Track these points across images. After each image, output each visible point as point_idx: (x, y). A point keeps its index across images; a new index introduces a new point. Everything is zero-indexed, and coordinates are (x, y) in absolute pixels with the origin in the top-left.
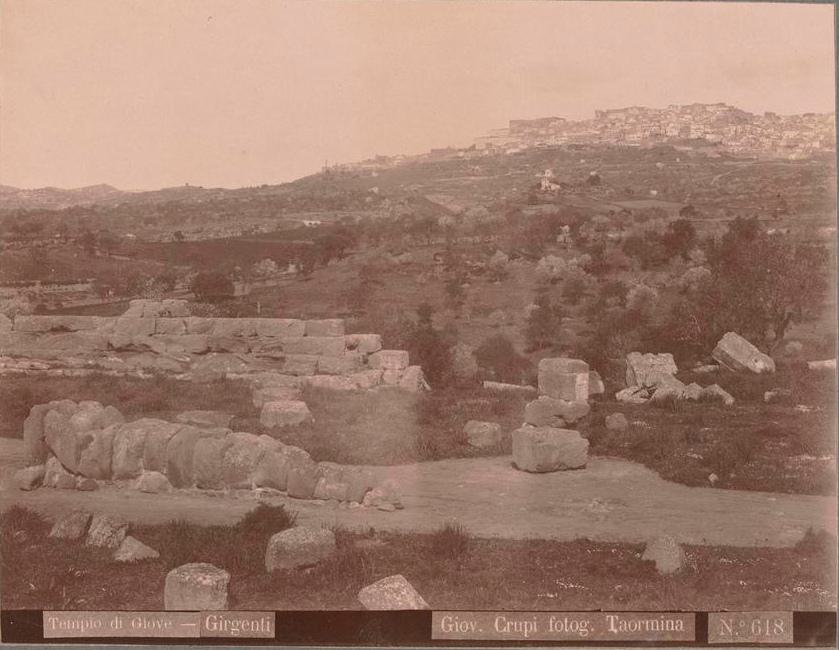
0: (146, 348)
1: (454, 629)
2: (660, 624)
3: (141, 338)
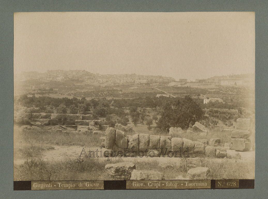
1: (136, 185)
2: (200, 184)
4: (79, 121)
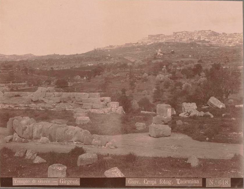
0: (43, 101)
1: (132, 183)
2: (192, 181)
3: (41, 98)
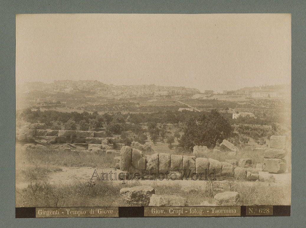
1: (156, 212)
2: (228, 210)
4: (90, 138)
